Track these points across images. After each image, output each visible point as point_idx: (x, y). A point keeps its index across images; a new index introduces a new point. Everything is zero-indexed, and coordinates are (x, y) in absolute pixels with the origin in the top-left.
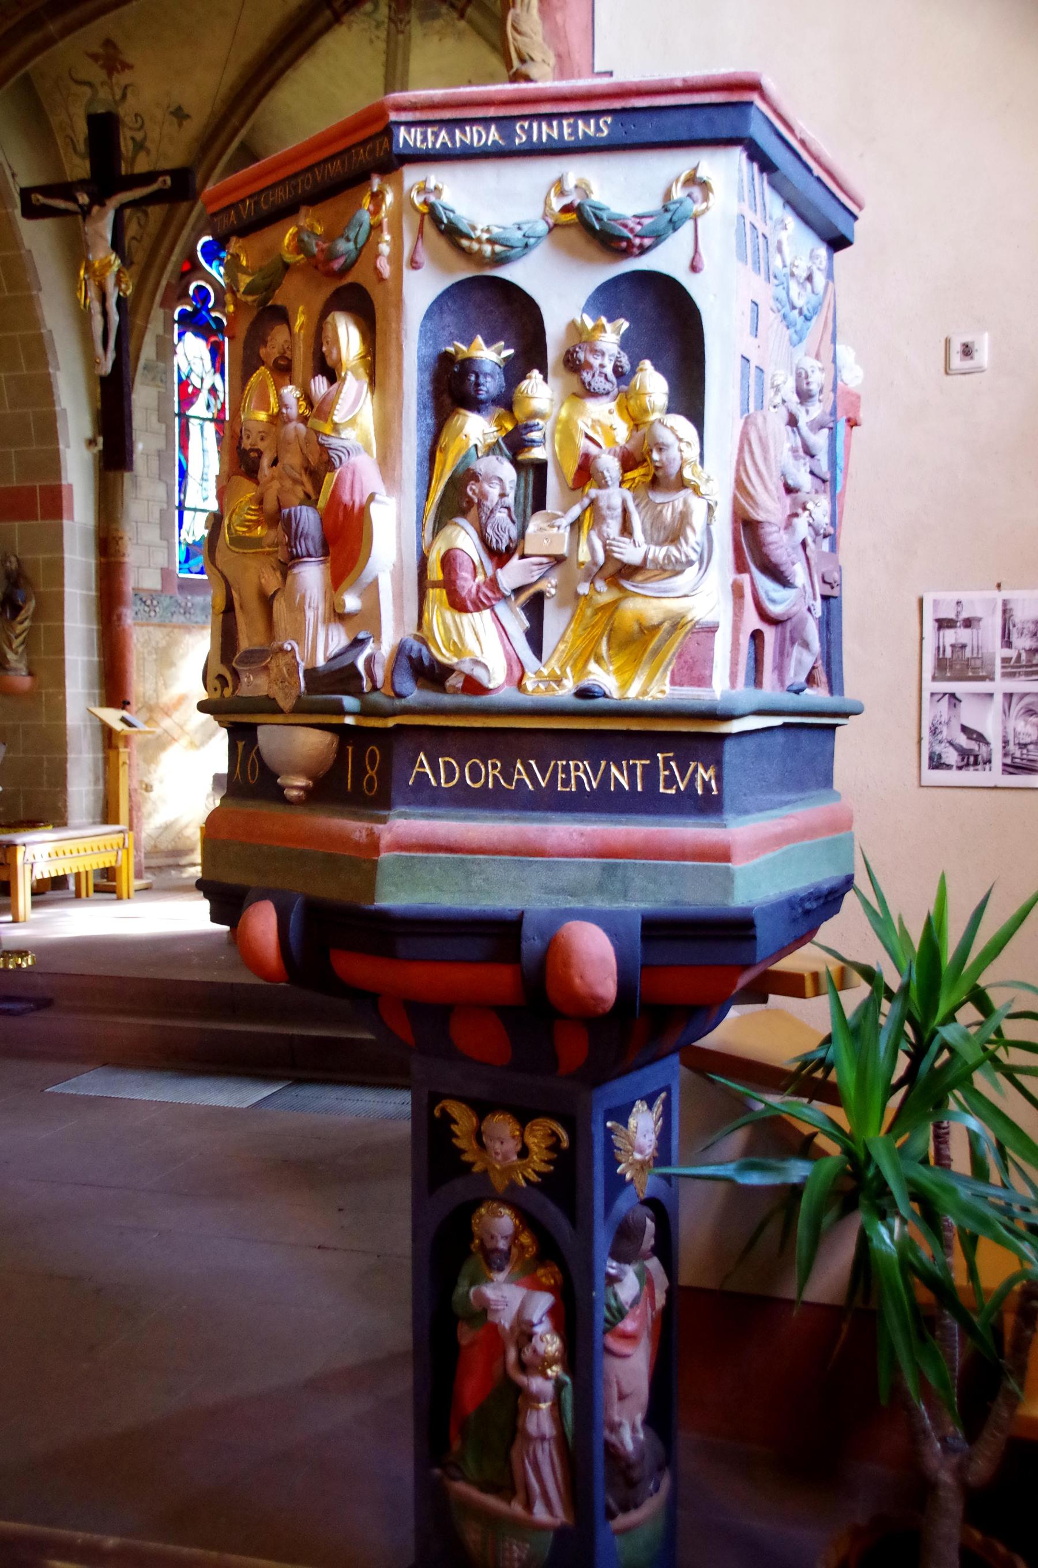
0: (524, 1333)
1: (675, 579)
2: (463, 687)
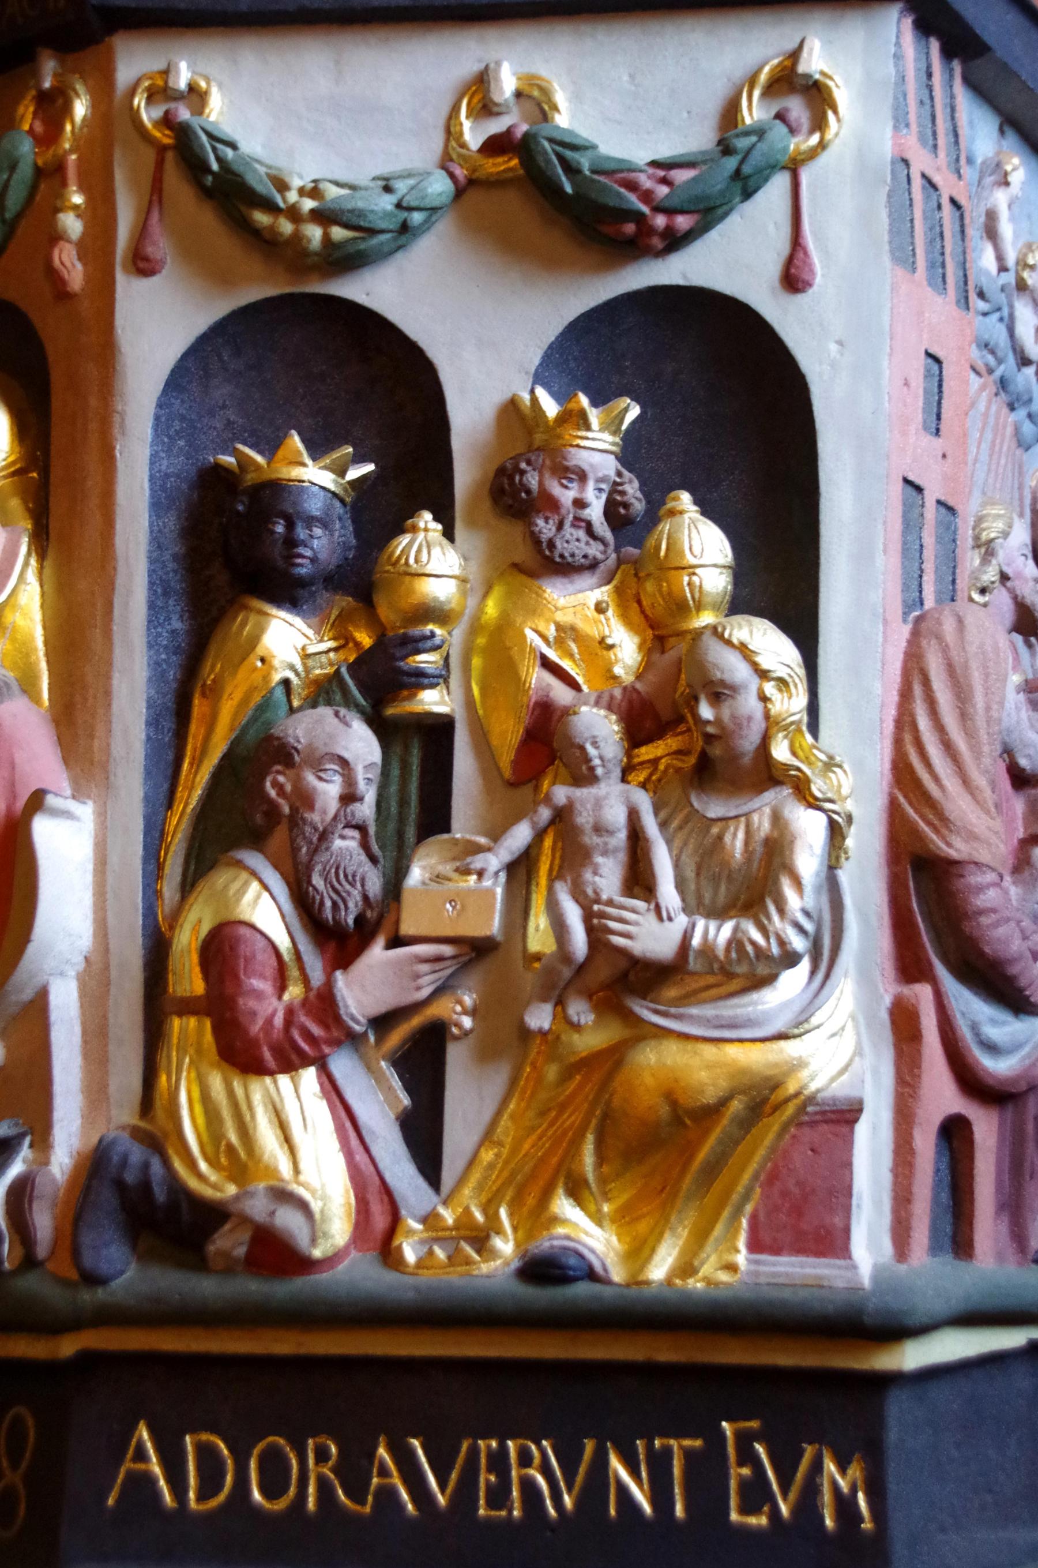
1: (755, 996)
2: (249, 1253)
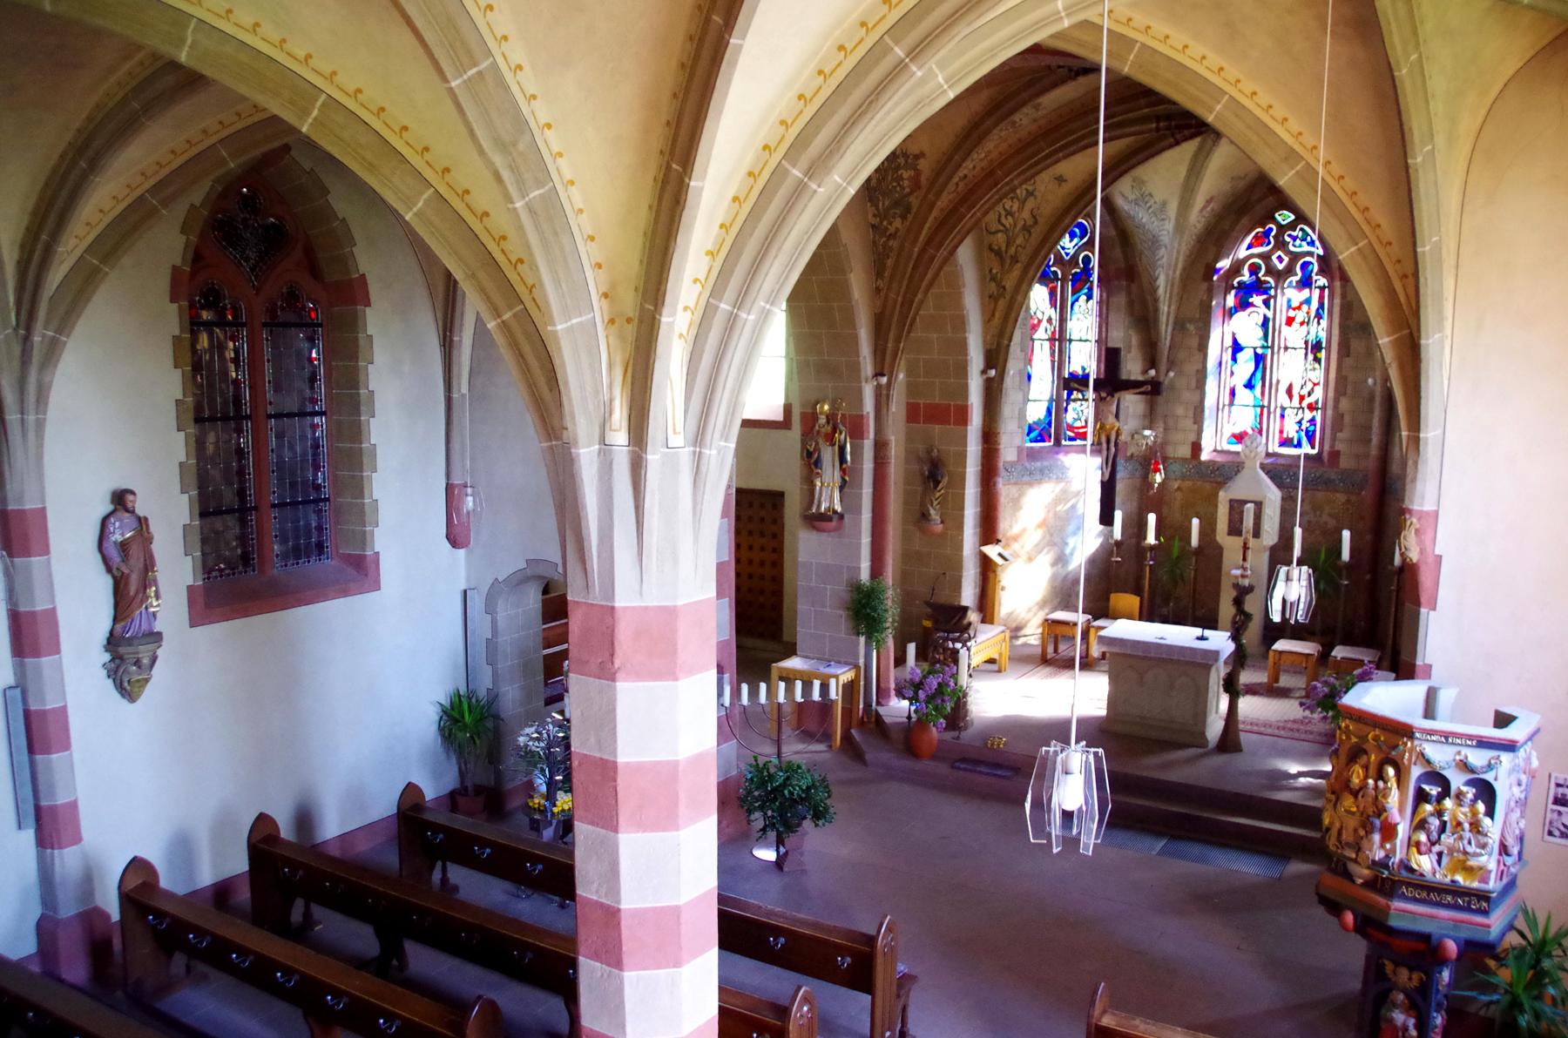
0: (1406, 1029)
